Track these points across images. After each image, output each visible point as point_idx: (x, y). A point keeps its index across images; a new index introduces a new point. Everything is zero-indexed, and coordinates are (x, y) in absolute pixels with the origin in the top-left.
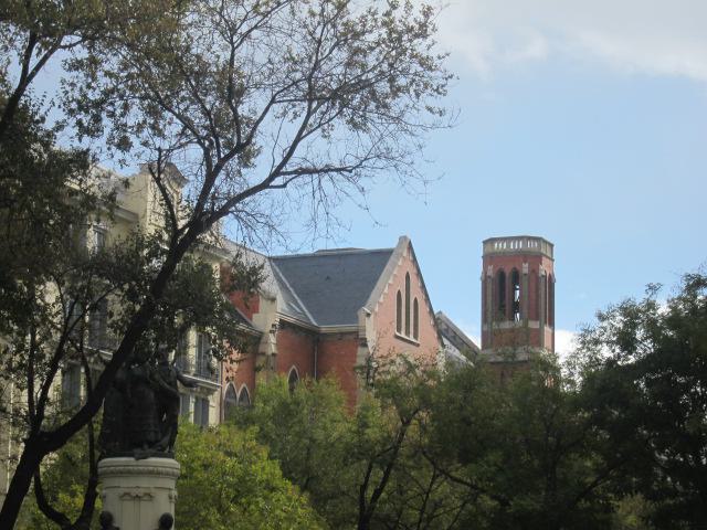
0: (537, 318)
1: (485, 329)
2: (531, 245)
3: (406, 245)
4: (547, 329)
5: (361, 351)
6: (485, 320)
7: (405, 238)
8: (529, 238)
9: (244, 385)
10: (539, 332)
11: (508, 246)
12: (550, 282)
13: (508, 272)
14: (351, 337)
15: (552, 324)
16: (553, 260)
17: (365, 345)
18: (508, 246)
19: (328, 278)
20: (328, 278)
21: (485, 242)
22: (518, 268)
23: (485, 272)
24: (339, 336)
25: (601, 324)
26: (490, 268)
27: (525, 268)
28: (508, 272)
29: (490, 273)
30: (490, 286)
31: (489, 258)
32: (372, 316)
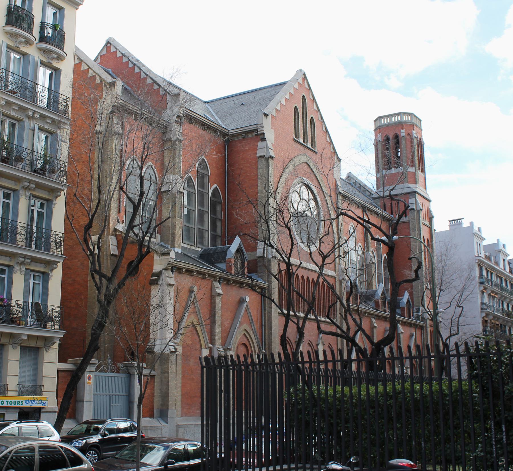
0: (413, 164)
1: (379, 175)
2: (406, 118)
3: (301, 75)
4: (420, 173)
5: (260, 144)
6: (378, 170)
7: (301, 70)
8: (405, 114)
9: (215, 185)
10: (414, 174)
11: (391, 120)
12: (421, 145)
13: (391, 137)
14: (252, 135)
15: (423, 171)
16: (422, 130)
17: (264, 139)
18: (391, 120)
19: (242, 104)
20: (242, 104)
21: (375, 121)
22: (398, 133)
23: (376, 139)
24: (243, 135)
25: (143, 435)
26: (380, 135)
27: (403, 133)
28: (391, 137)
29: (380, 138)
30: (380, 147)
31: (378, 129)
32: (269, 117)
